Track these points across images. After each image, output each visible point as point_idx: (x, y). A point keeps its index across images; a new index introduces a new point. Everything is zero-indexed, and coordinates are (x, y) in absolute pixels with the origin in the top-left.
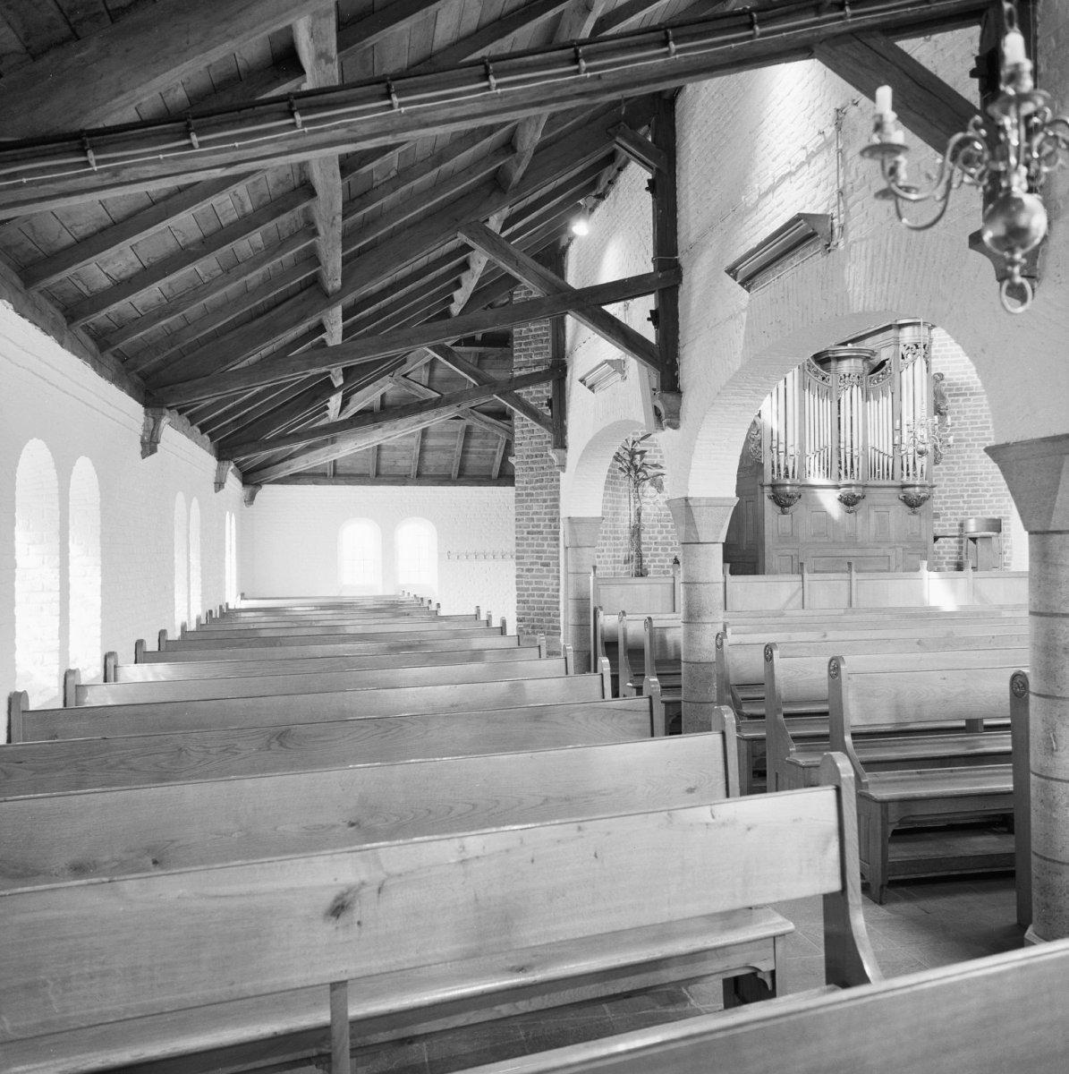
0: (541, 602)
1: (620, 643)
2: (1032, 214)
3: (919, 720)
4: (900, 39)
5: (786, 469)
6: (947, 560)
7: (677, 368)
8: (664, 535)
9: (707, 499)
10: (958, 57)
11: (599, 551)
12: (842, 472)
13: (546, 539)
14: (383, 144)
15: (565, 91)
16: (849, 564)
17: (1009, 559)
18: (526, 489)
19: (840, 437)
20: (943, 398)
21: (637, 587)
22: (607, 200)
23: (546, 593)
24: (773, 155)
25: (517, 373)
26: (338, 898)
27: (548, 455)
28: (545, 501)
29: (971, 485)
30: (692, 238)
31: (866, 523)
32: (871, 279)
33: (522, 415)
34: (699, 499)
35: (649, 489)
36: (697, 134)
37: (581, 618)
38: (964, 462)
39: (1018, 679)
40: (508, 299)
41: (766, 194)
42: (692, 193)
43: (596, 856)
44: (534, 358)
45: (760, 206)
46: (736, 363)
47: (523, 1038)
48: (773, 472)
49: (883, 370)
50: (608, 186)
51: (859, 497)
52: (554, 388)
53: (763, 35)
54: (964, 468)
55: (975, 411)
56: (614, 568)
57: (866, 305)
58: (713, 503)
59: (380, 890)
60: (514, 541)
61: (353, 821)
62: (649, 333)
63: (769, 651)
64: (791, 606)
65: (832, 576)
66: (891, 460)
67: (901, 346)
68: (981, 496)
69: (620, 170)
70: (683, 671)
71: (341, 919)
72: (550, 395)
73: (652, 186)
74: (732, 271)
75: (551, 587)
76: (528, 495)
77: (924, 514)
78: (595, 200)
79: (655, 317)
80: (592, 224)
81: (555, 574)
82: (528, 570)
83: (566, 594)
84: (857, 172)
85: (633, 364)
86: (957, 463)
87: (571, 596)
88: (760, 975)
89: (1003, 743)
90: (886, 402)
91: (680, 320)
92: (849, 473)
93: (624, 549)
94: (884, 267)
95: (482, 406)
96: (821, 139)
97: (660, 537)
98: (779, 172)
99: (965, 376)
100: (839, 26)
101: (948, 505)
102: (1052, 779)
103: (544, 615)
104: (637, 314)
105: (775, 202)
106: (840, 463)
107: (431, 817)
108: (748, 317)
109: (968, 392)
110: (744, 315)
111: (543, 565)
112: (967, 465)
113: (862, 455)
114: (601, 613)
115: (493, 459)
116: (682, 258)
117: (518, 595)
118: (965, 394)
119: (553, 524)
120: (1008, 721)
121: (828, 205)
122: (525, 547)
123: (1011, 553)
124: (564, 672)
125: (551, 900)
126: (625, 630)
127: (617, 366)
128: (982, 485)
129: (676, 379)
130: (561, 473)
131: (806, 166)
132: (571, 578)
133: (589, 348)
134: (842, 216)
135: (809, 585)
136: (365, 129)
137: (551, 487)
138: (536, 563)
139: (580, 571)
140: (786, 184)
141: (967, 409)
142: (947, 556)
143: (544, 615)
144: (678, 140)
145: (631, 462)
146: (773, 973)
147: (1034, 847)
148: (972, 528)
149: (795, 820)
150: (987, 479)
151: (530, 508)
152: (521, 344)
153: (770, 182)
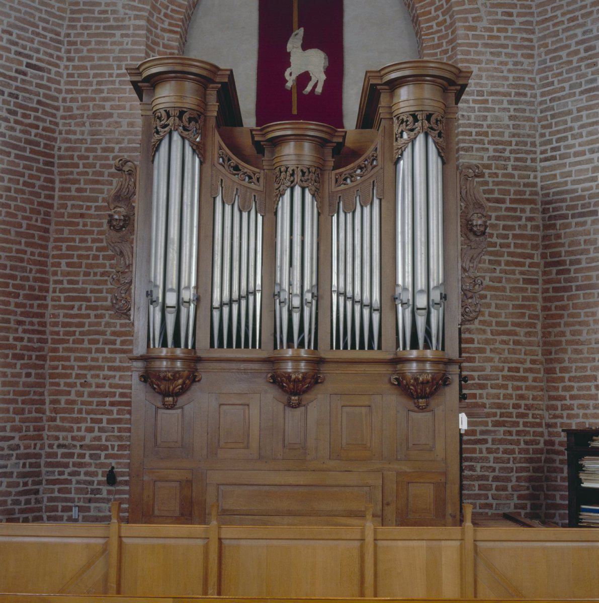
8: (96, 433)
66: (376, 316)
90: (369, 217)
97: (89, 436)
101: (575, 392)
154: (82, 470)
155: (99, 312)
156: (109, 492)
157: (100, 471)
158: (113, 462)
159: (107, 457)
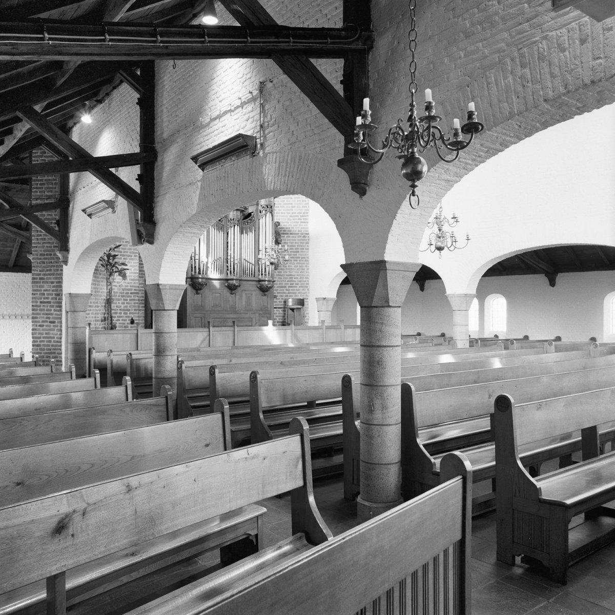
0: (49, 346)
1: (108, 369)
2: (423, 166)
3: (294, 402)
4: (313, 58)
5: (199, 269)
6: (278, 320)
7: (153, 210)
8: (126, 305)
9: (170, 285)
10: (329, 71)
11: (87, 314)
12: (229, 272)
13: (53, 306)
14: (29, 59)
15: (147, 51)
16: (234, 322)
17: (308, 319)
18: (39, 275)
19: (227, 253)
20: (279, 235)
21: (115, 335)
22: (103, 104)
23: (52, 340)
24: (220, 99)
25: (34, 202)
26: (60, 522)
27: (55, 254)
28: (52, 283)
29: (290, 281)
30: (165, 135)
31: (240, 300)
32: (279, 173)
33: (39, 229)
34: (165, 285)
35: (117, 278)
36: (169, 77)
37: (77, 354)
38: (287, 269)
39: (346, 379)
40: (28, 155)
41: (215, 119)
42: (165, 110)
43: (195, 481)
44: (46, 193)
45: (211, 125)
46: (194, 210)
47: (109, 601)
48: (192, 271)
49: (250, 218)
50: (105, 96)
51: (237, 286)
52: (61, 213)
53: (252, 42)
54: (287, 272)
55: (292, 243)
56: (95, 324)
57: (275, 187)
58: (174, 287)
59: (84, 514)
60: (30, 307)
61: (19, 481)
62: (136, 186)
63: (212, 370)
64: (203, 346)
65: (224, 328)
66: (253, 267)
67: (260, 206)
68: (294, 287)
69: (114, 88)
70: (153, 383)
71: (62, 534)
72: (57, 218)
73: (140, 102)
74: (195, 159)
75: (56, 336)
76: (40, 279)
77: (269, 296)
78: (95, 103)
79: (140, 178)
80: (91, 116)
81: (59, 328)
82: (40, 326)
83: (67, 342)
84: (271, 117)
85: (122, 204)
86: (283, 269)
87: (70, 341)
88: (251, 538)
89: (339, 410)
90: (251, 235)
91: (155, 182)
92: (232, 273)
93: (100, 312)
94: (286, 168)
95: (8, 221)
96: (250, 96)
97: (123, 306)
98: (223, 109)
99: (288, 224)
100: (286, 46)
102: (372, 425)
103: (51, 353)
104: (129, 175)
105: (221, 125)
106: (228, 267)
107: (68, 474)
108: (201, 185)
109: (300, 233)
110: (199, 184)
111: (51, 322)
112: (288, 271)
113: (240, 263)
114: (94, 351)
115: (10, 255)
116: (158, 146)
117: (33, 342)
118: (287, 234)
119: (58, 297)
120: (340, 399)
121: (254, 131)
122: (38, 312)
123: (308, 316)
124: (94, 387)
125: (174, 507)
126: (112, 361)
127: (110, 204)
128: (295, 281)
129: (152, 216)
130: (64, 266)
131: (241, 108)
132: (70, 330)
133: (90, 190)
134: (262, 138)
135: (213, 334)
136: (24, 49)
137: (57, 274)
138: (46, 322)
139: (76, 326)
140: (228, 115)
141: (289, 241)
142: (278, 318)
143: (51, 353)
144: (156, 78)
145: (108, 261)
146: (257, 536)
147: (361, 458)
148: (290, 303)
149: (284, 453)
150: (297, 278)
151: (43, 287)
152: (37, 184)
153: (218, 113)
154: (121, 319)
155: (125, 257)
156: (131, 327)
157: (127, 319)
158: (132, 315)
159: (130, 313)
